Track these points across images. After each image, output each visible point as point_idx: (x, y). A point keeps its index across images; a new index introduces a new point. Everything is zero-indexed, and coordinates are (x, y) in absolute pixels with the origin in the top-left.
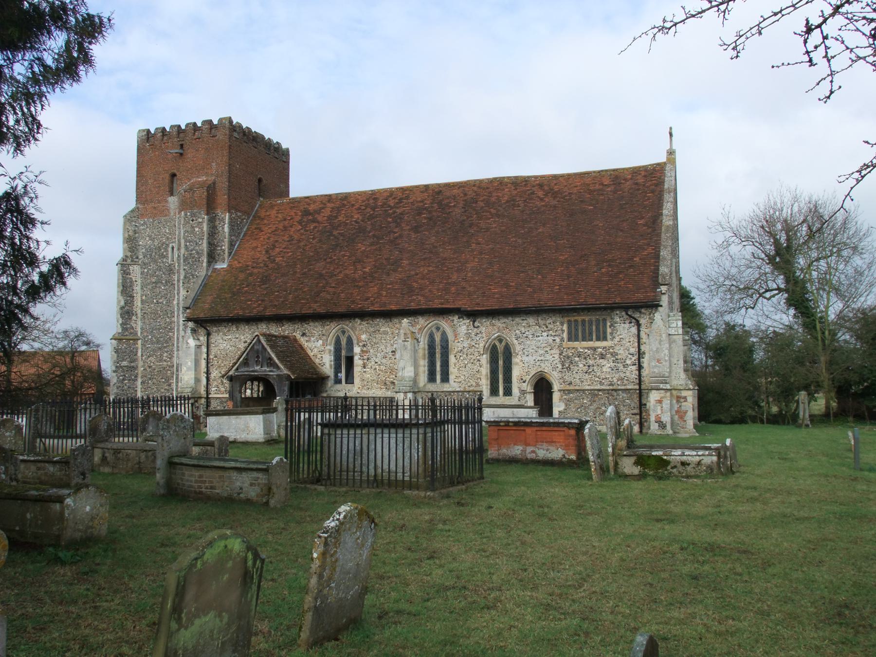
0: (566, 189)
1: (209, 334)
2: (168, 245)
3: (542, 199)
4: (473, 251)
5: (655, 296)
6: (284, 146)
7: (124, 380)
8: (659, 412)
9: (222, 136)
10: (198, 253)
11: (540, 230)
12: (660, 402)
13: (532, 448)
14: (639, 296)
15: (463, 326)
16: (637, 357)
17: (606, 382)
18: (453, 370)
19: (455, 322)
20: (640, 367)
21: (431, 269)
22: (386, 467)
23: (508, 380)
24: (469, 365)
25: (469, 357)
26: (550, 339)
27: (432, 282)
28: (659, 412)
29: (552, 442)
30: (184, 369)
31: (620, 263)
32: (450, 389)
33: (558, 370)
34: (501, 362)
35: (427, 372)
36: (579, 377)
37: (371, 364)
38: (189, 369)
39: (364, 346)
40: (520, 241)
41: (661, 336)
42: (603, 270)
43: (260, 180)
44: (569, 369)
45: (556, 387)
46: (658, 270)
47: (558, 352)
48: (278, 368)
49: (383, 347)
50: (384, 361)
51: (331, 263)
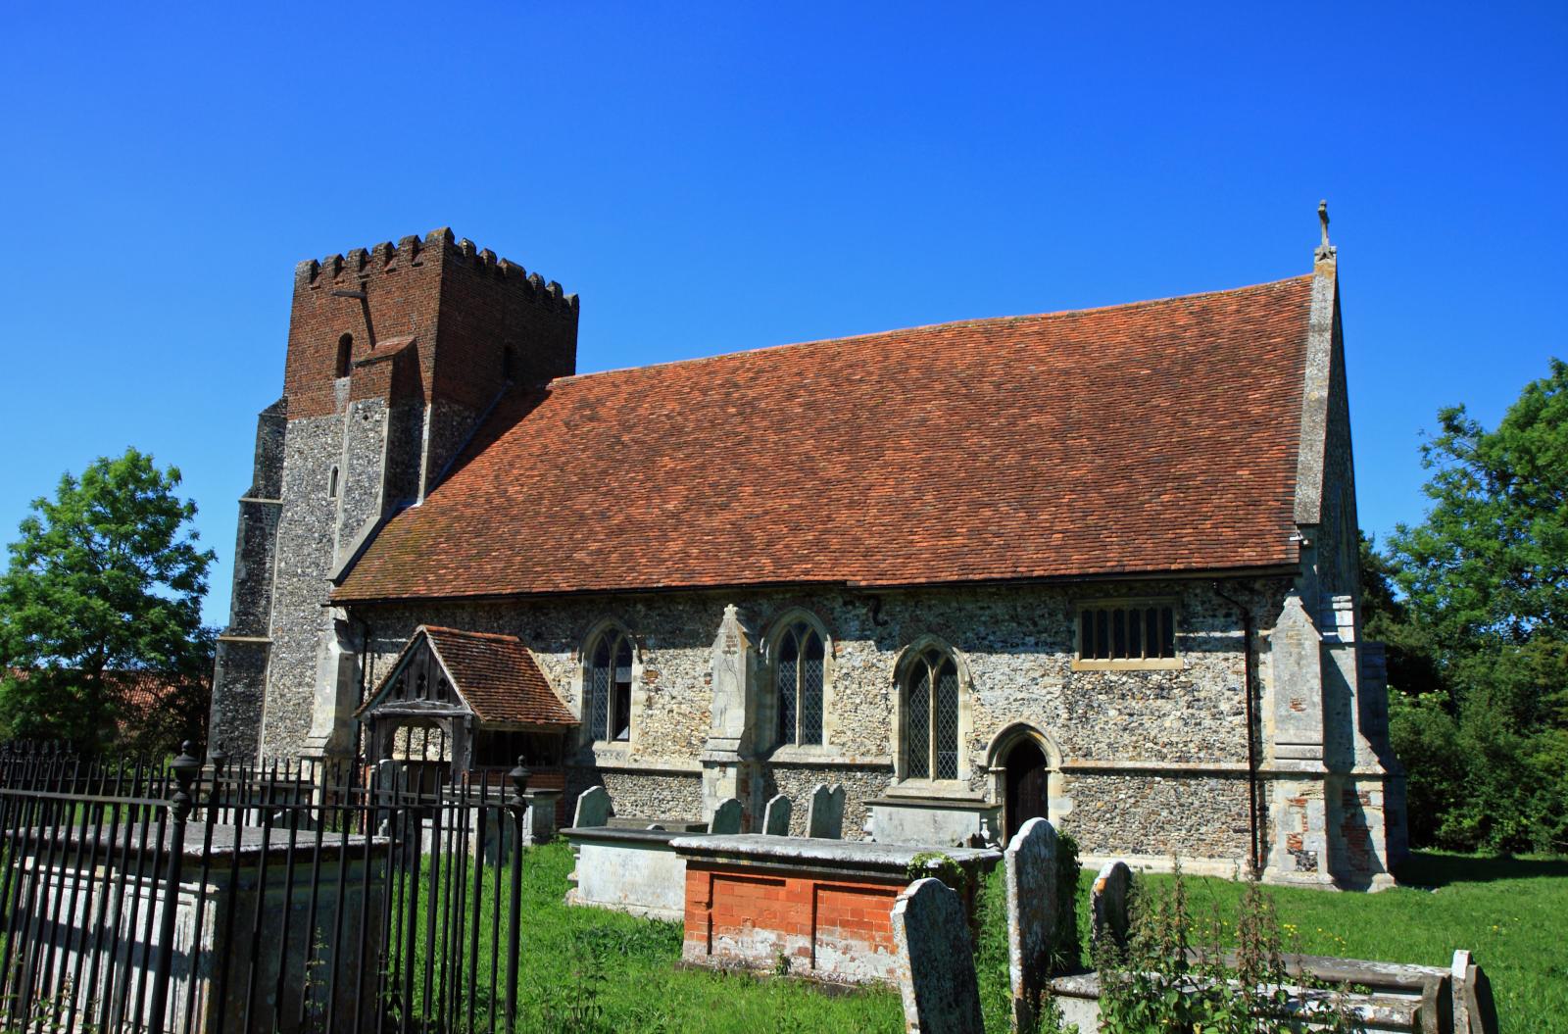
0: (1094, 338)
2: (328, 467)
3: (1041, 361)
4: (886, 464)
7: (234, 718)
8: (1299, 829)
9: (432, 262)
11: (1033, 421)
12: (1300, 802)
16: (1243, 696)
18: (829, 719)
21: (796, 501)
24: (864, 706)
27: (796, 529)
28: (1299, 829)
29: (861, 924)
30: (318, 700)
31: (1204, 482)
33: (1060, 722)
36: (1109, 738)
37: (662, 700)
38: (326, 700)
40: (987, 442)
41: (1300, 644)
42: (1165, 498)
43: (508, 350)
44: (1084, 719)
45: (1054, 763)
46: (1292, 493)
48: (457, 702)
50: (689, 694)
51: (605, 494)
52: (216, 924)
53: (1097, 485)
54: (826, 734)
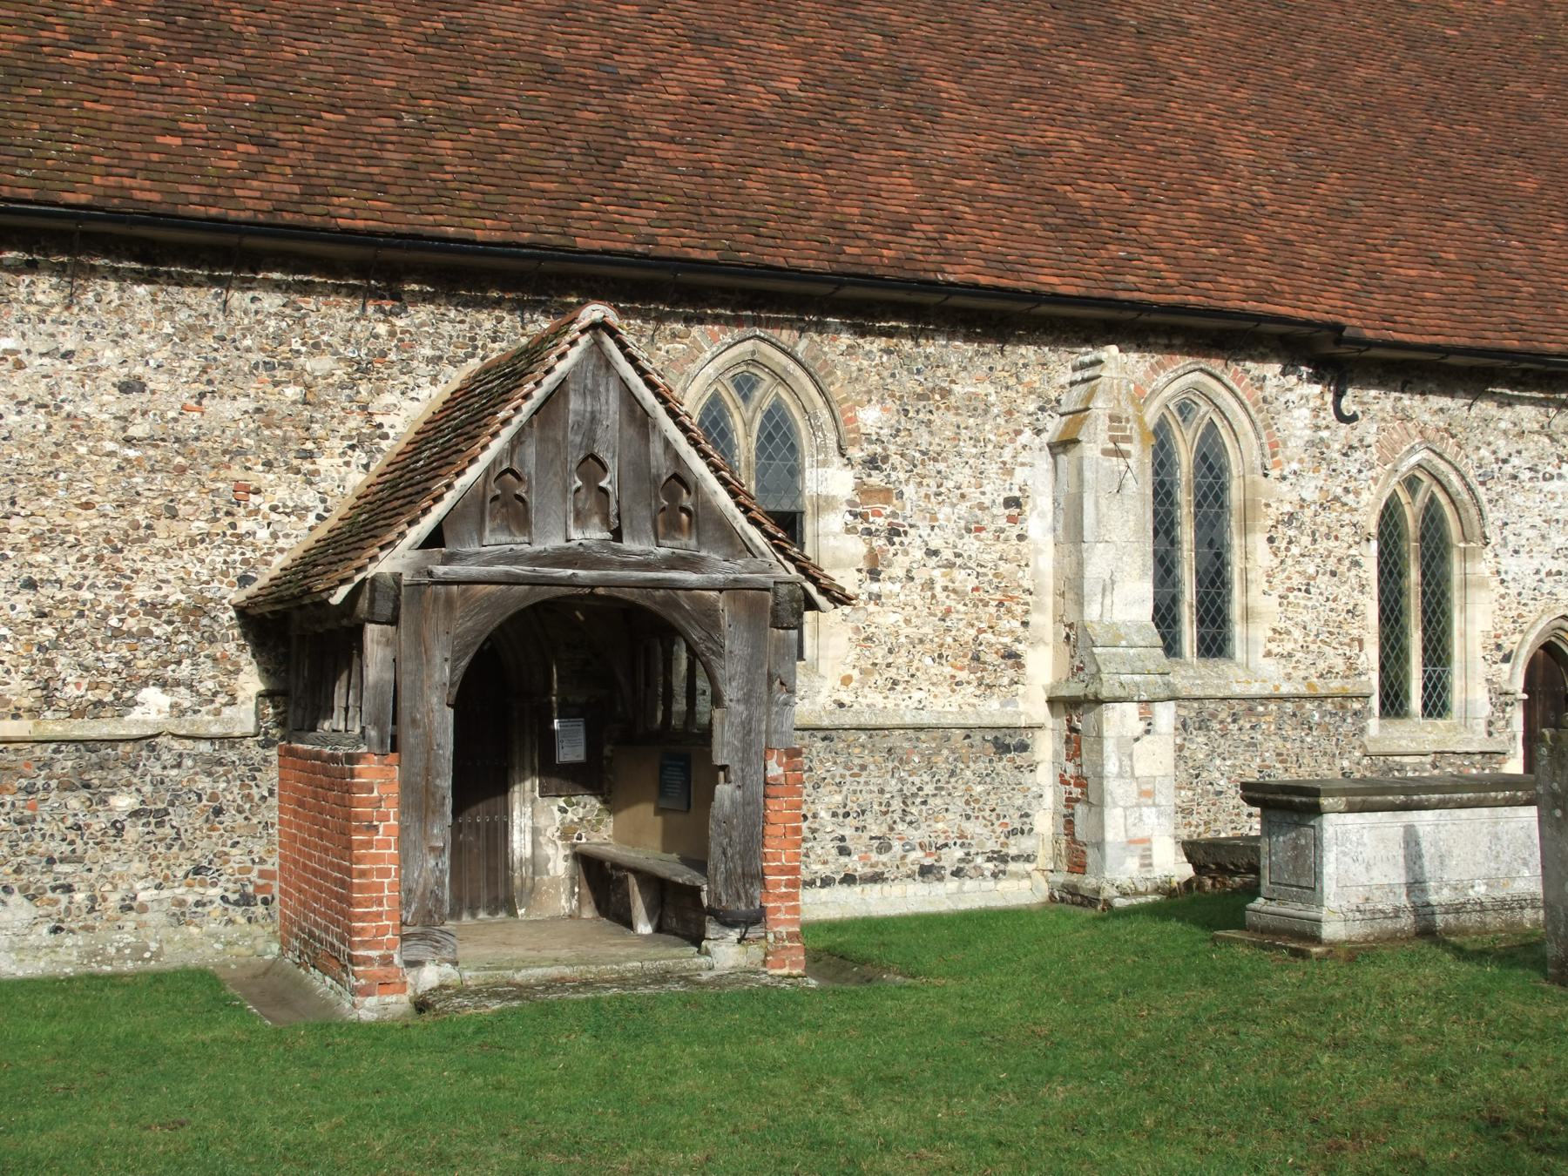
15: (1297, 400)
19: (1270, 388)
20: (826, 882)
23: (1438, 652)
25: (1323, 545)
32: (1255, 689)
34: (1414, 575)
39: (872, 463)
49: (963, 476)
50: (970, 545)
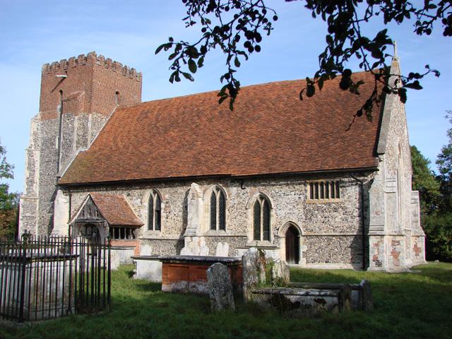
1: (70, 196)
5: (374, 163)
6: (138, 71)
10: (70, 141)
13: (193, 284)
14: (362, 164)
17: (338, 230)
21: (215, 147)
22: (90, 293)
26: (297, 197)
28: (376, 253)
31: (350, 139)
35: (147, 217)
36: (317, 226)
47: (303, 206)
52: (310, 270)
53: (316, 140)
54: (227, 226)
